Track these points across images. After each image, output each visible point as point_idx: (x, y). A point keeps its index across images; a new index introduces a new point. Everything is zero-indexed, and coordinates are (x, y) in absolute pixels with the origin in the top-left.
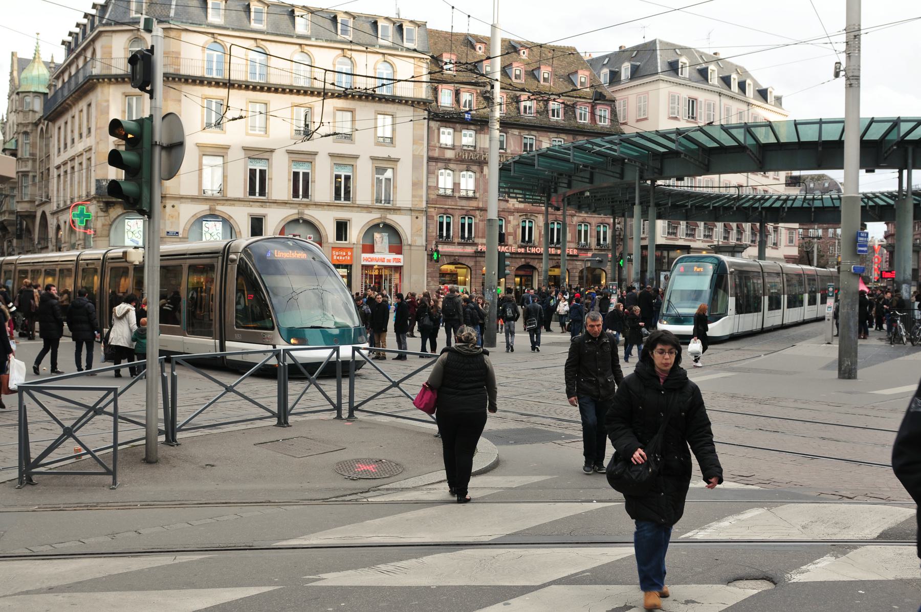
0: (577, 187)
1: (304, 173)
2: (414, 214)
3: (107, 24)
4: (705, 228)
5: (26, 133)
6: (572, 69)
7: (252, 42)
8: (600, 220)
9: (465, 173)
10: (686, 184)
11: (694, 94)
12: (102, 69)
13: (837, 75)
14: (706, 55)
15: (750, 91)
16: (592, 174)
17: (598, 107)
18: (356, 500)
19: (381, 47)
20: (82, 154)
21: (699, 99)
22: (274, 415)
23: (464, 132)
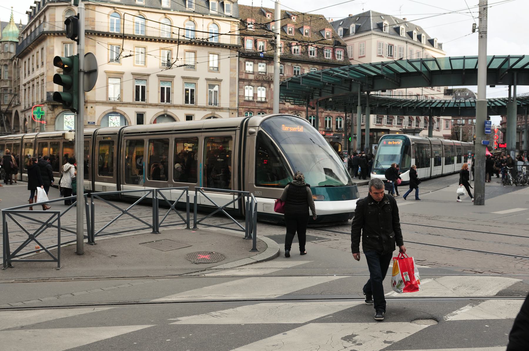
1: (142, 86)
4: (398, 119)
6: (322, 28)
7: (137, 12)
9: (260, 88)
11: (392, 42)
12: (50, 27)
13: (474, 31)
14: (399, 19)
15: (424, 40)
16: (333, 88)
17: (337, 50)
19: (211, 15)
20: (38, 77)
21: (395, 45)
23: (259, 64)
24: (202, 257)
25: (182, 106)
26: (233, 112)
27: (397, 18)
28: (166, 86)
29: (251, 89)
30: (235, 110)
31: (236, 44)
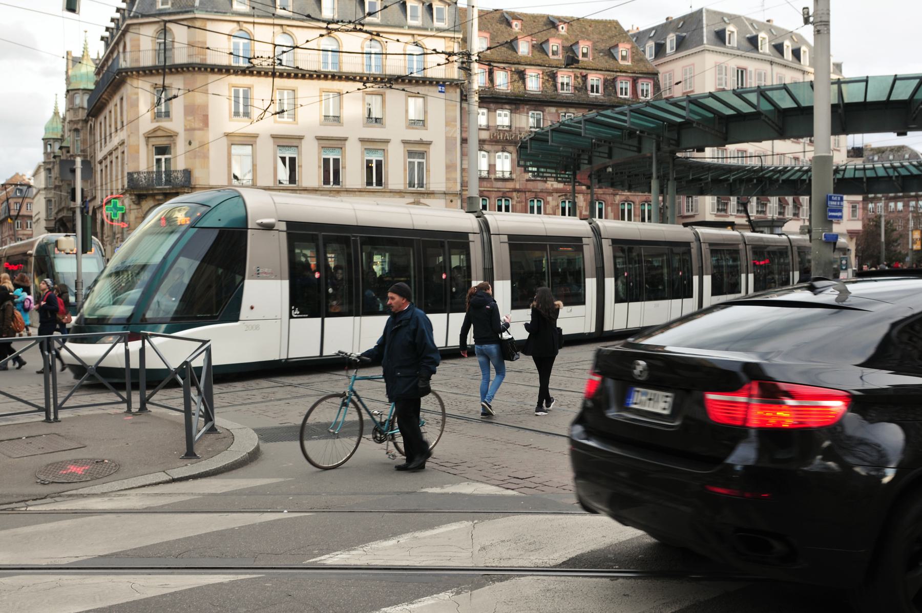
0: (598, 162)
1: (290, 158)
2: (449, 198)
3: (135, 17)
4: (757, 203)
5: (76, 130)
6: (613, 42)
7: (235, 25)
8: (644, 198)
9: (500, 154)
10: (709, 155)
11: (743, 63)
12: (132, 61)
14: (757, 22)
16: (610, 149)
17: (640, 81)
18: (13, 509)
19: (410, 27)
20: (117, 148)
21: (749, 69)
22: (40, 409)
23: (498, 112)
24: (72, 469)
25: (360, 191)
26: (451, 198)
27: (754, 21)
28: (331, 156)
29: (506, 157)
30: (455, 194)
31: (456, 77)
